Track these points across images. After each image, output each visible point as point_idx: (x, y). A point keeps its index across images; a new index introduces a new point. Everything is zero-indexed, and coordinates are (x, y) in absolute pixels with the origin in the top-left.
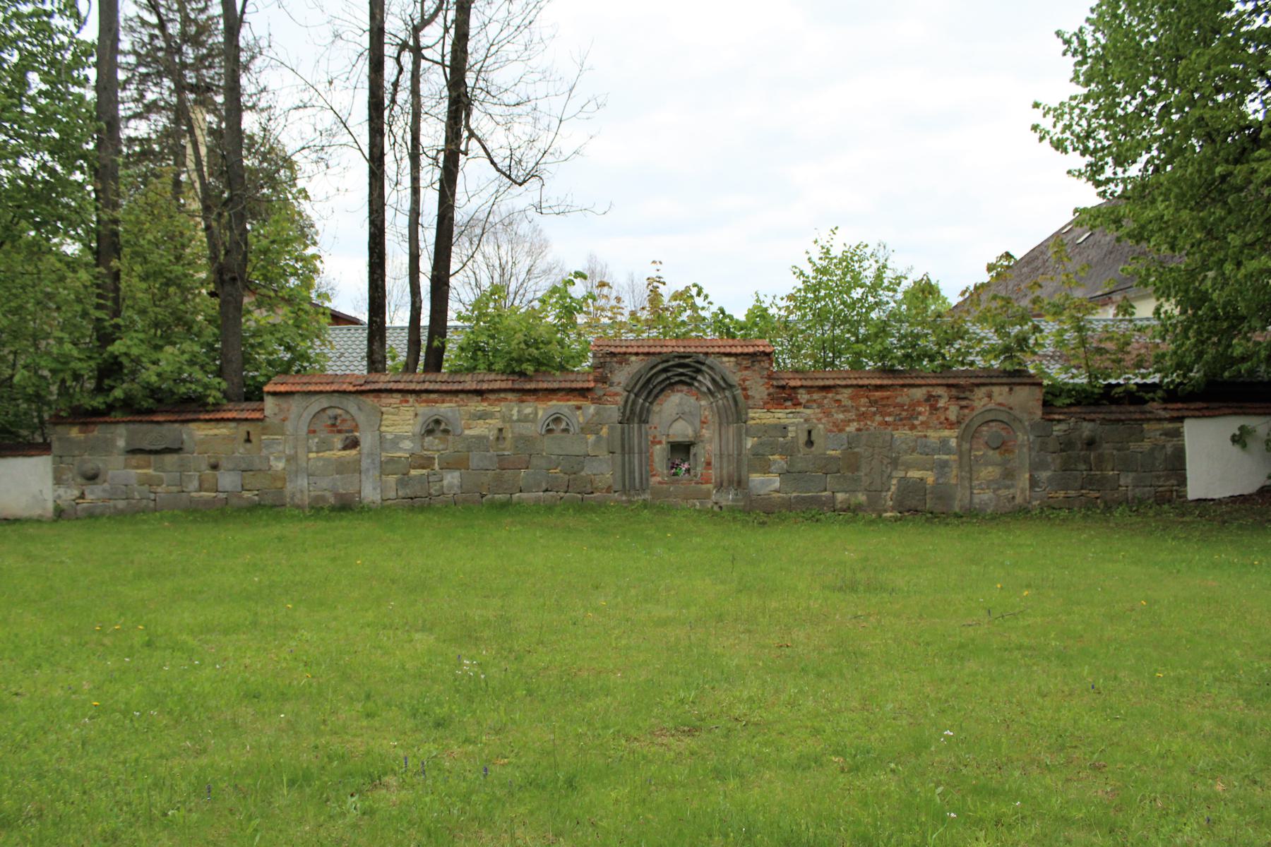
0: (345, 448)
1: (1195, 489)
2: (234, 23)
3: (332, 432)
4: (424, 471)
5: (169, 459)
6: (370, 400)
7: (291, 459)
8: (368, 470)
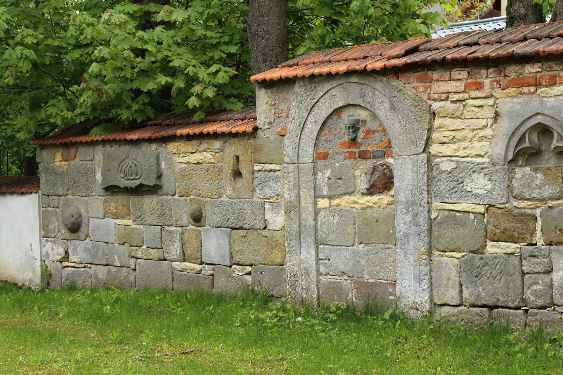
0: (371, 190)
1: (489, 244)
2: (2, 281)
3: (351, 156)
4: (512, 247)
5: (149, 203)
6: (410, 87)
7: (293, 209)
8: (406, 236)
